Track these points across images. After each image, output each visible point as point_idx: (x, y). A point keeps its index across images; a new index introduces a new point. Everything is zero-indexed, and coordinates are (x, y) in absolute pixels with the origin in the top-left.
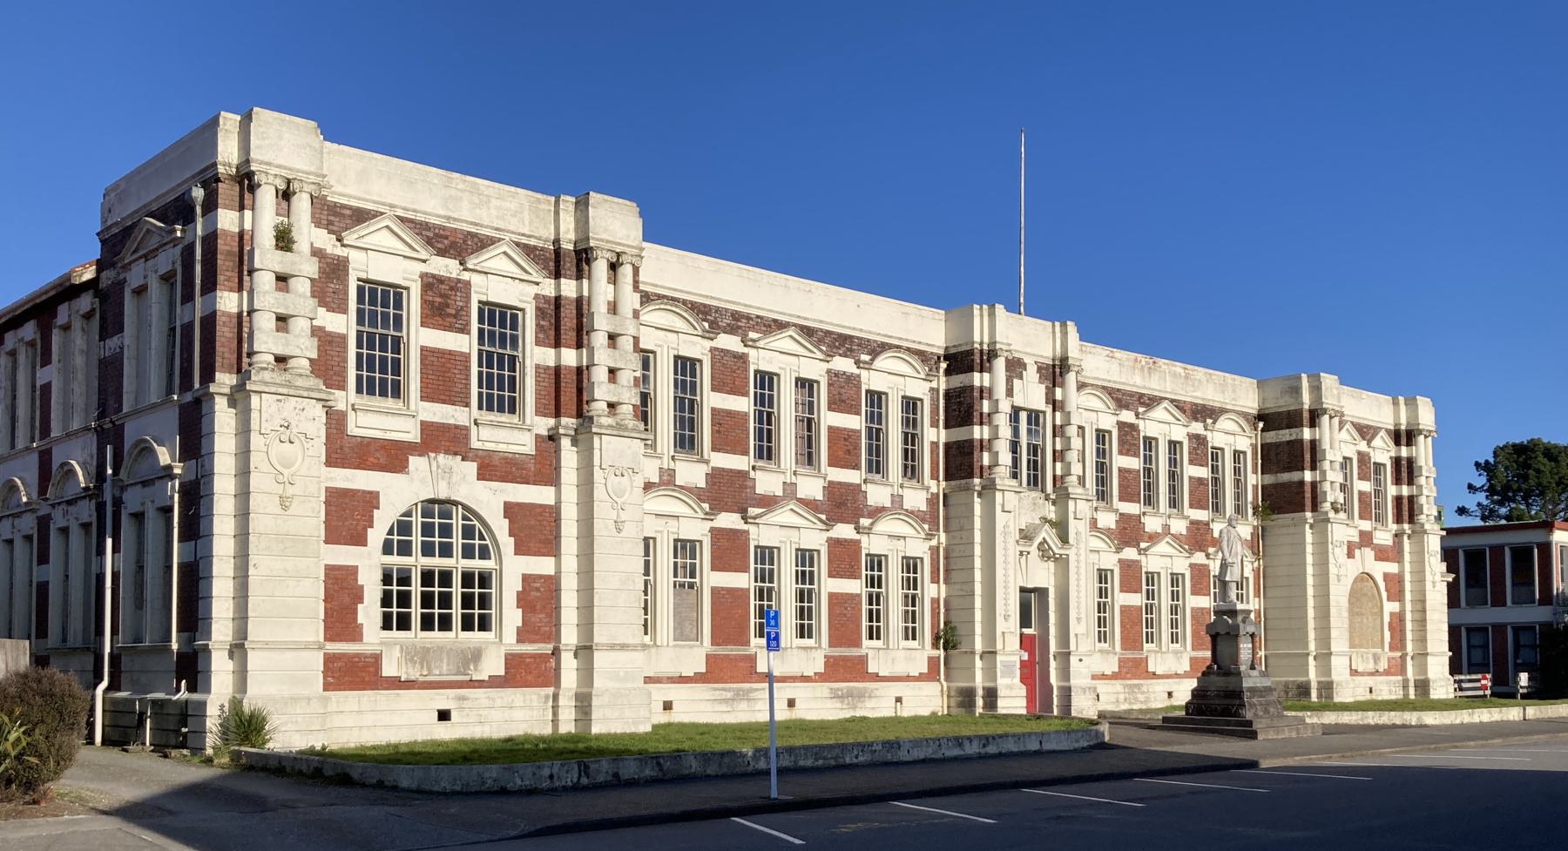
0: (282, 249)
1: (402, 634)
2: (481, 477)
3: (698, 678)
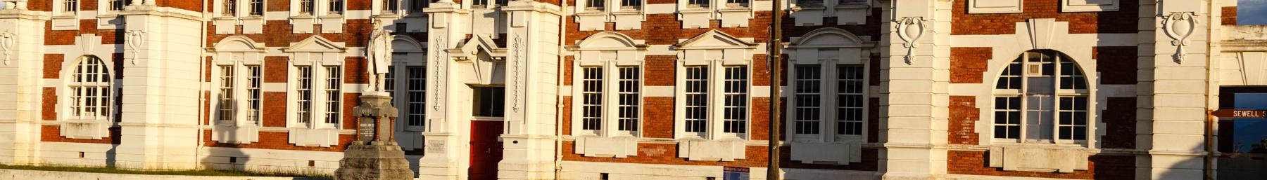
2: (1071, 31)
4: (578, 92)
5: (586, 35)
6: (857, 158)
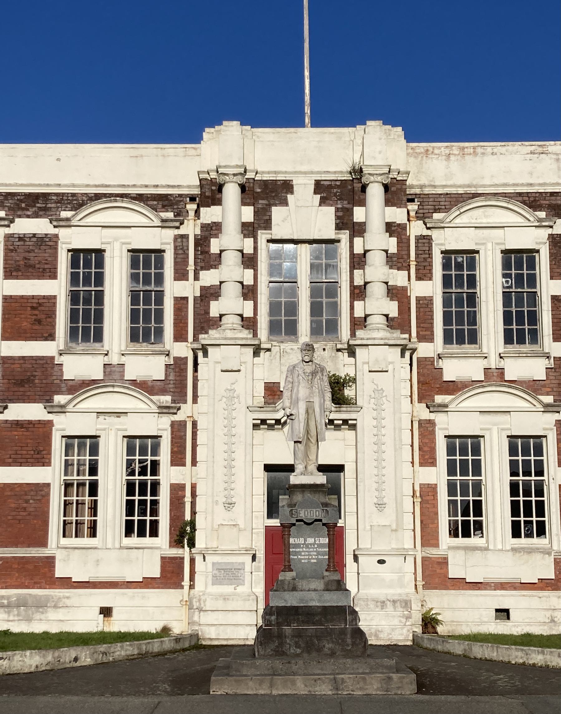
0: (364, 231)
1: (466, 540)
3: (147, 583)
4: (437, 475)
5: (454, 388)
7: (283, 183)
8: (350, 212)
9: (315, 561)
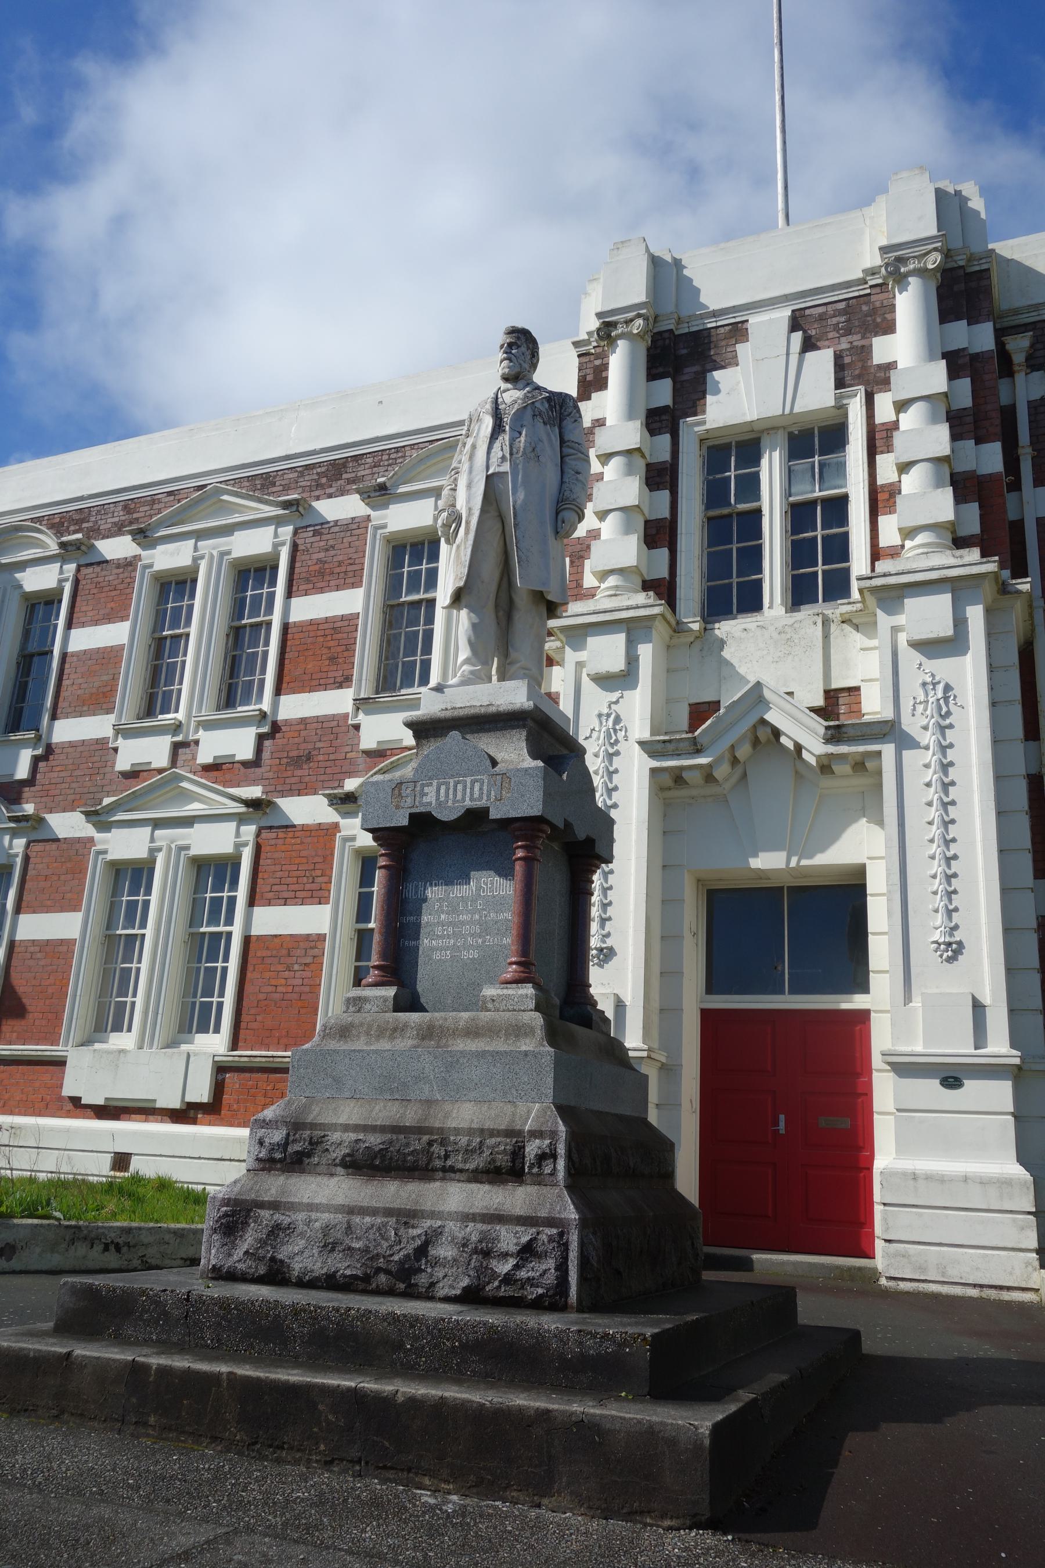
6: (201, 1092)
7: (730, 331)
8: (866, 351)
9: (474, 954)
